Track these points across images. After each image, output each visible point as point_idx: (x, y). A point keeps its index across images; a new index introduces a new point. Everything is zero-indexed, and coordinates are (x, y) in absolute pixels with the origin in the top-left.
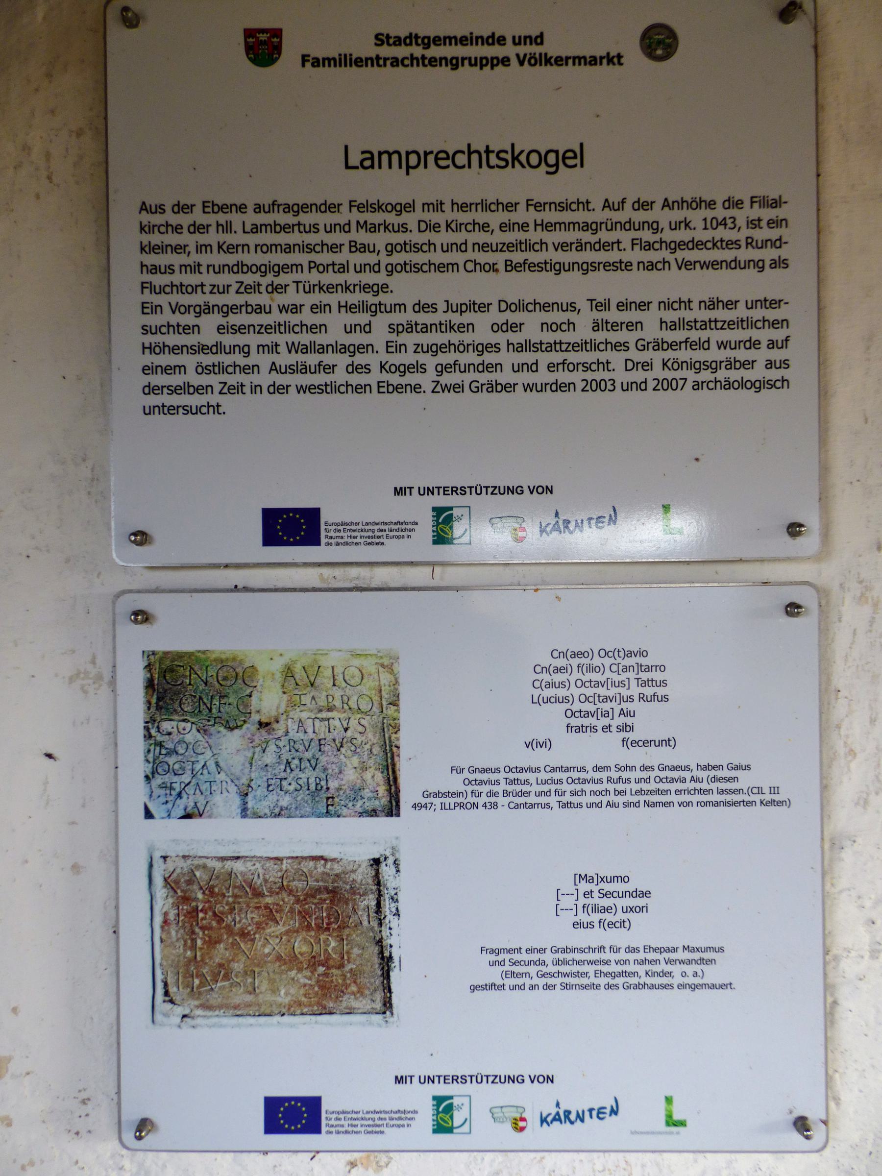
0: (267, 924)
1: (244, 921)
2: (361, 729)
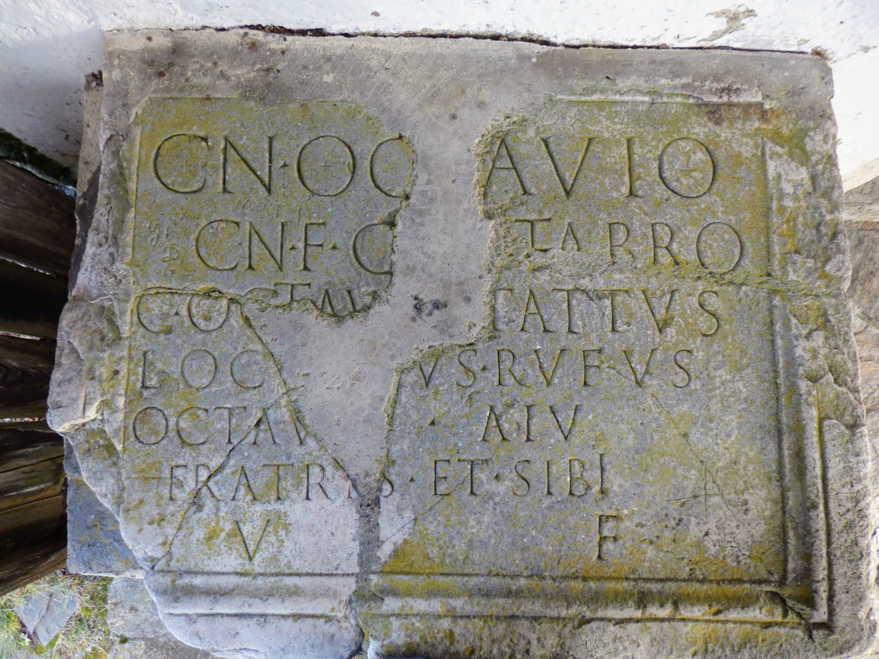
2: (705, 323)
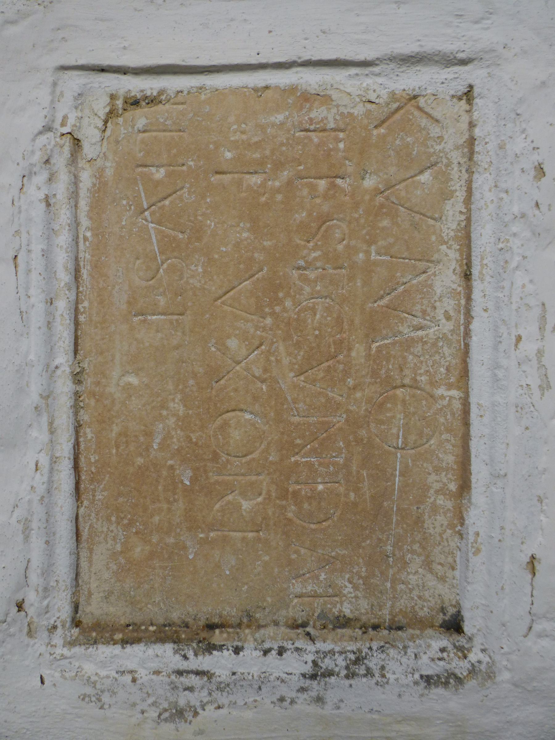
0: (298, 345)
1: (308, 289)
